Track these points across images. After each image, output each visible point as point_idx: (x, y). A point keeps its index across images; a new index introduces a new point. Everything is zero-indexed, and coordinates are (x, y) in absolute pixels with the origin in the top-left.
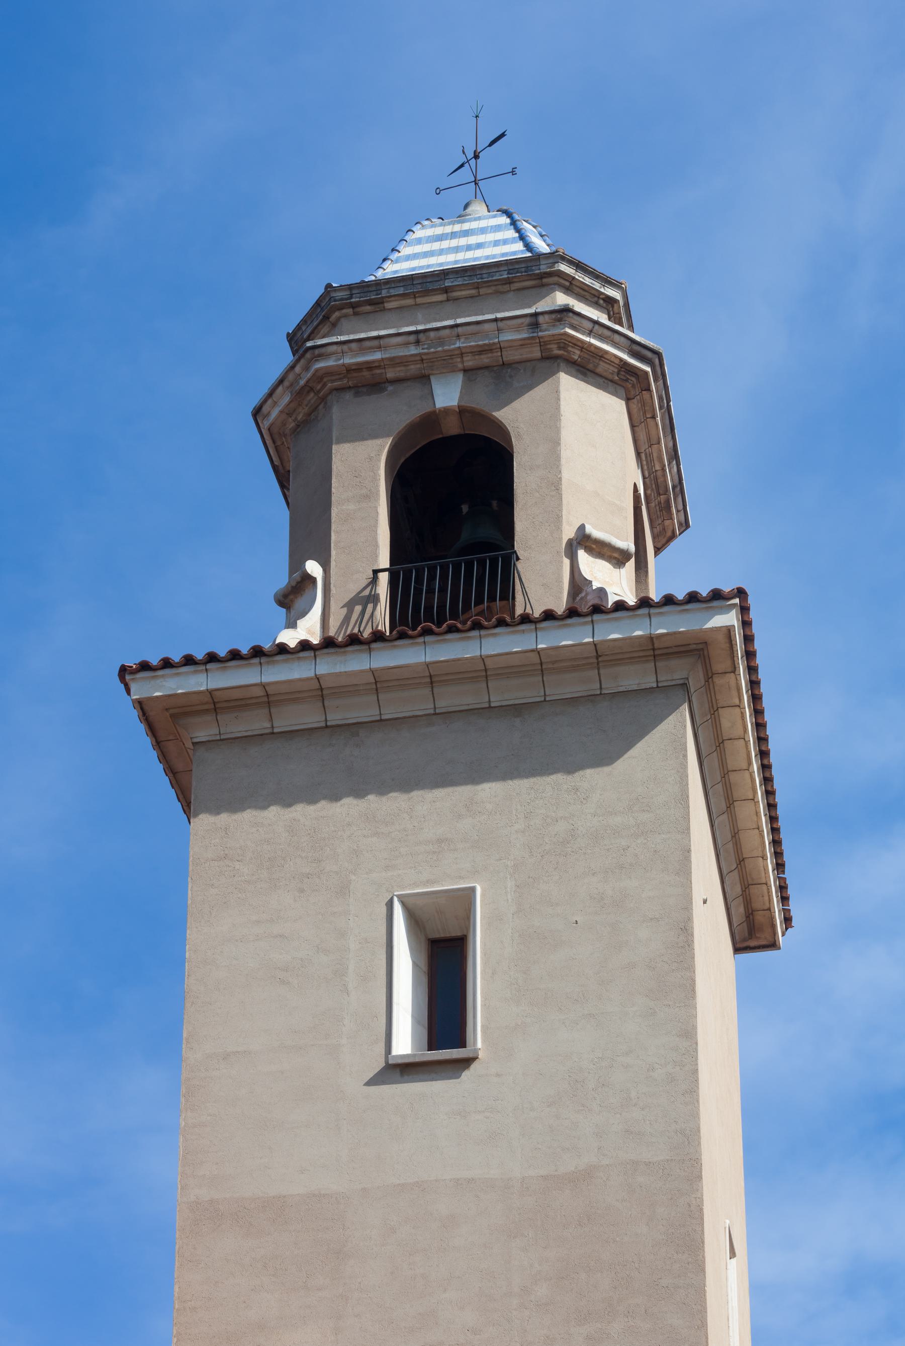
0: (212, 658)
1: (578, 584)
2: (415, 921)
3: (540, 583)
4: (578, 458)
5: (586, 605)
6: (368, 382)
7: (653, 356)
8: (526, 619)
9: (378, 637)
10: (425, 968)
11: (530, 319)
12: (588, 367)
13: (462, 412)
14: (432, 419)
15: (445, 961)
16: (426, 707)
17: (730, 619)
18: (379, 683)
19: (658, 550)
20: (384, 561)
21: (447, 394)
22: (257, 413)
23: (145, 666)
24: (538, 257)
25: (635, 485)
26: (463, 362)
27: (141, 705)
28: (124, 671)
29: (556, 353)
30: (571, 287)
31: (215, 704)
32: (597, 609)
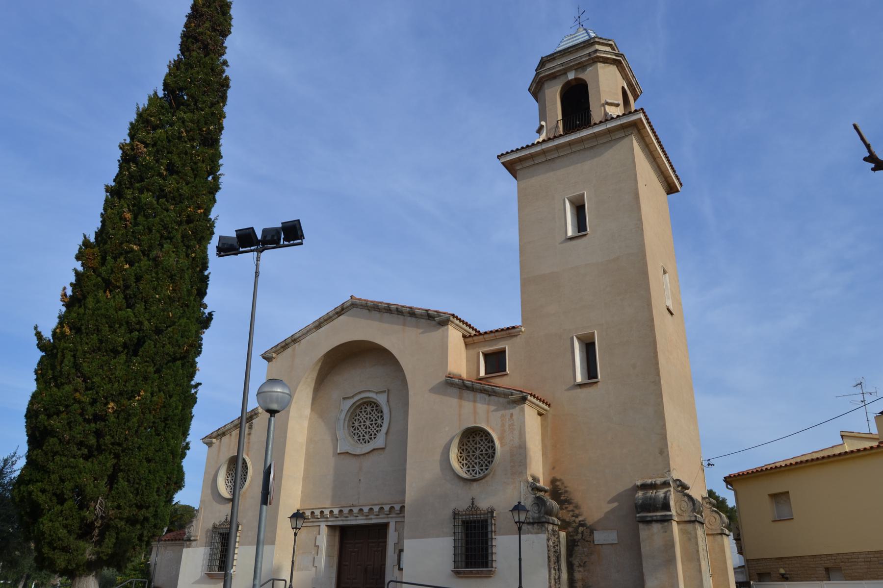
0: (517, 149)
1: (606, 114)
2: (571, 202)
3: (596, 115)
4: (607, 85)
5: (608, 119)
6: (553, 77)
7: (622, 55)
8: (595, 124)
9: (561, 135)
10: (575, 212)
11: (585, 54)
12: (606, 61)
13: (576, 79)
14: (569, 83)
15: (580, 210)
16: (544, 159)
17: (642, 116)
18: (557, 148)
19: (635, 100)
20: (560, 117)
21: (571, 76)
22: (529, 90)
23: (503, 154)
24: (591, 38)
25: (623, 88)
26: (166, 132)
27: (503, 163)
28: (498, 157)
29: (596, 60)
30: (599, 43)
31: (520, 160)
32: (612, 118)
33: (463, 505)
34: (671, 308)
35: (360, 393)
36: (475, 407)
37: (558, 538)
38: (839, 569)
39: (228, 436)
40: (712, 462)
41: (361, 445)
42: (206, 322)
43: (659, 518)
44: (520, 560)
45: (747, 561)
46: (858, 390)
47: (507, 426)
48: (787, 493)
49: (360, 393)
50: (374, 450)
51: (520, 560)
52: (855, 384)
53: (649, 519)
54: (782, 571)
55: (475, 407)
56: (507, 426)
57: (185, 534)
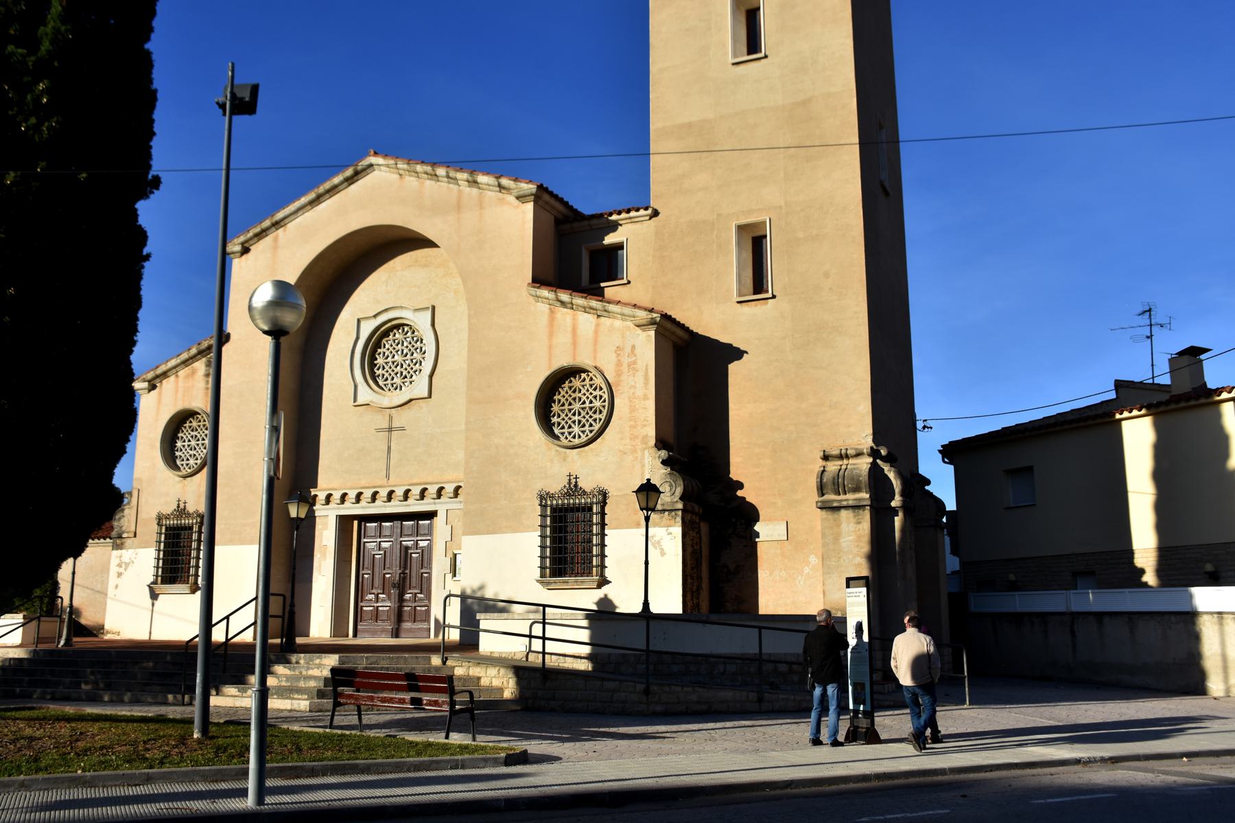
33: (556, 485)
34: (887, 185)
35: (386, 310)
36: (574, 319)
37: (699, 532)
38: (1092, 573)
39: (172, 378)
40: (929, 424)
41: (389, 393)
42: (148, 257)
43: (851, 503)
44: (647, 563)
45: (962, 564)
46: (1145, 320)
47: (625, 365)
48: (1029, 469)
49: (386, 310)
50: (411, 400)
51: (647, 563)
52: (1141, 310)
53: (835, 504)
54: (1012, 577)
55: (574, 319)
56: (625, 365)
57: (112, 528)
